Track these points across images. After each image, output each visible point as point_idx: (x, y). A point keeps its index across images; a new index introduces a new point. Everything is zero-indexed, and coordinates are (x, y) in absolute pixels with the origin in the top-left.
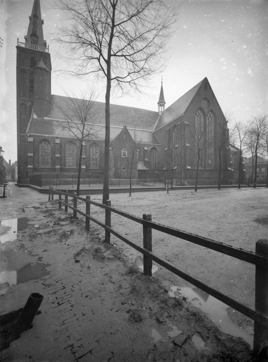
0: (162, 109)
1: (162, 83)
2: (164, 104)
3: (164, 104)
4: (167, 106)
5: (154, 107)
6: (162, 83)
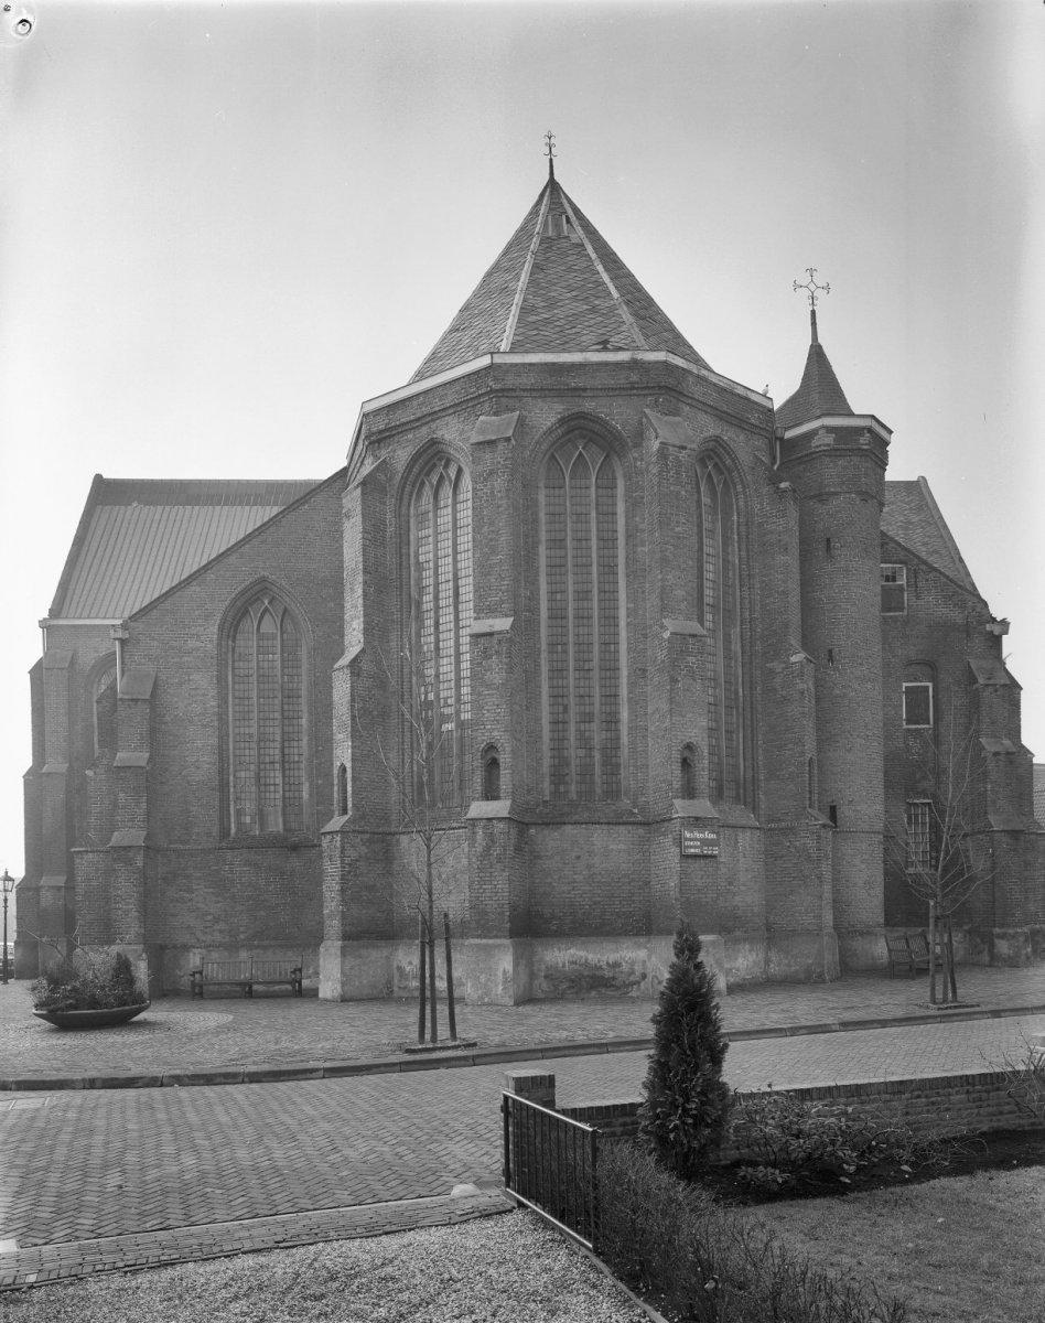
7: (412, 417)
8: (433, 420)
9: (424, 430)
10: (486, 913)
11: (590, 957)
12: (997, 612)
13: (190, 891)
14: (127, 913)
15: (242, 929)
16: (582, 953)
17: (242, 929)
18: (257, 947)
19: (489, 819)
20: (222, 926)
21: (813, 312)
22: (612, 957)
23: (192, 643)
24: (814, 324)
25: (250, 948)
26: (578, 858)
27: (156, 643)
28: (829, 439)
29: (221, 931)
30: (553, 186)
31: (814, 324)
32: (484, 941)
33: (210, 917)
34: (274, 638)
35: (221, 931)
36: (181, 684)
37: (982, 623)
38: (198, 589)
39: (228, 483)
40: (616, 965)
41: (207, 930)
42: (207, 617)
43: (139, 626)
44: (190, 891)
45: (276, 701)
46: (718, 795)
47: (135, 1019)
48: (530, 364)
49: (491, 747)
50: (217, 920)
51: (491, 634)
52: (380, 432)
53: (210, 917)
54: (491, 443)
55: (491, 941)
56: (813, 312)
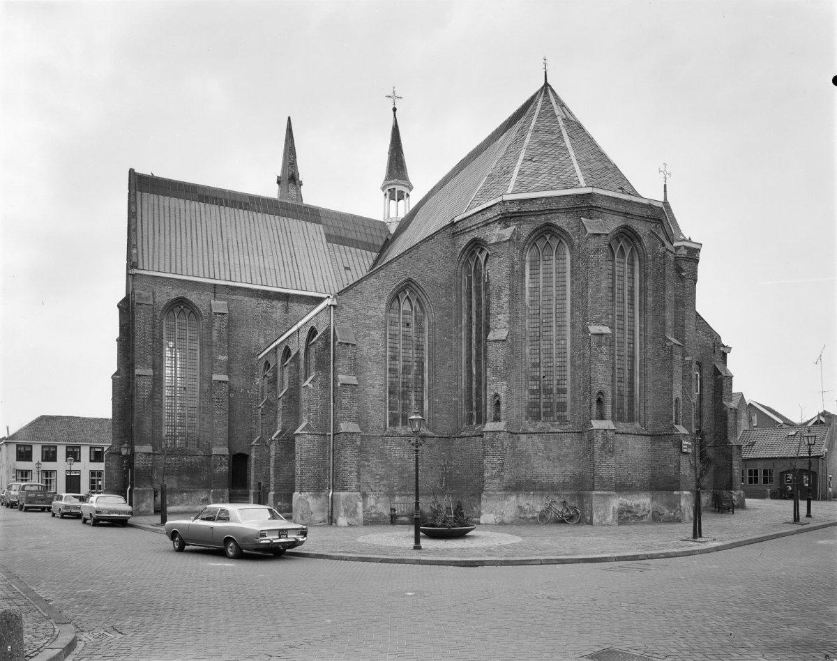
0: (401, 210)
1: (395, 110)
2: (406, 190)
3: (406, 190)
4: (415, 197)
5: (372, 205)
6: (395, 110)
7: (537, 209)
8: (550, 213)
9: (543, 218)
10: (603, 478)
11: (628, 501)
12: (724, 342)
13: (368, 460)
14: (351, 472)
15: (395, 484)
16: (625, 500)
17: (395, 484)
18: (405, 495)
19: (606, 430)
20: (385, 482)
21: (665, 185)
22: (637, 502)
23: (371, 313)
24: (665, 191)
25: (401, 495)
26: (623, 451)
27: (352, 310)
28: (685, 252)
29: (384, 485)
30: (546, 85)
31: (665, 191)
32: (602, 492)
33: (378, 477)
34: (410, 314)
35: (384, 485)
36: (365, 336)
37: (719, 347)
38: (375, 280)
39: (223, 192)
40: (638, 506)
41: (377, 484)
42: (380, 298)
43: (343, 299)
44: (368, 460)
45: (411, 351)
46: (613, 419)
47: (469, 534)
48: (608, 196)
49: (601, 393)
50: (382, 478)
51: (602, 335)
52: (514, 212)
53: (378, 477)
54: (598, 235)
55: (606, 493)
56: (665, 185)
